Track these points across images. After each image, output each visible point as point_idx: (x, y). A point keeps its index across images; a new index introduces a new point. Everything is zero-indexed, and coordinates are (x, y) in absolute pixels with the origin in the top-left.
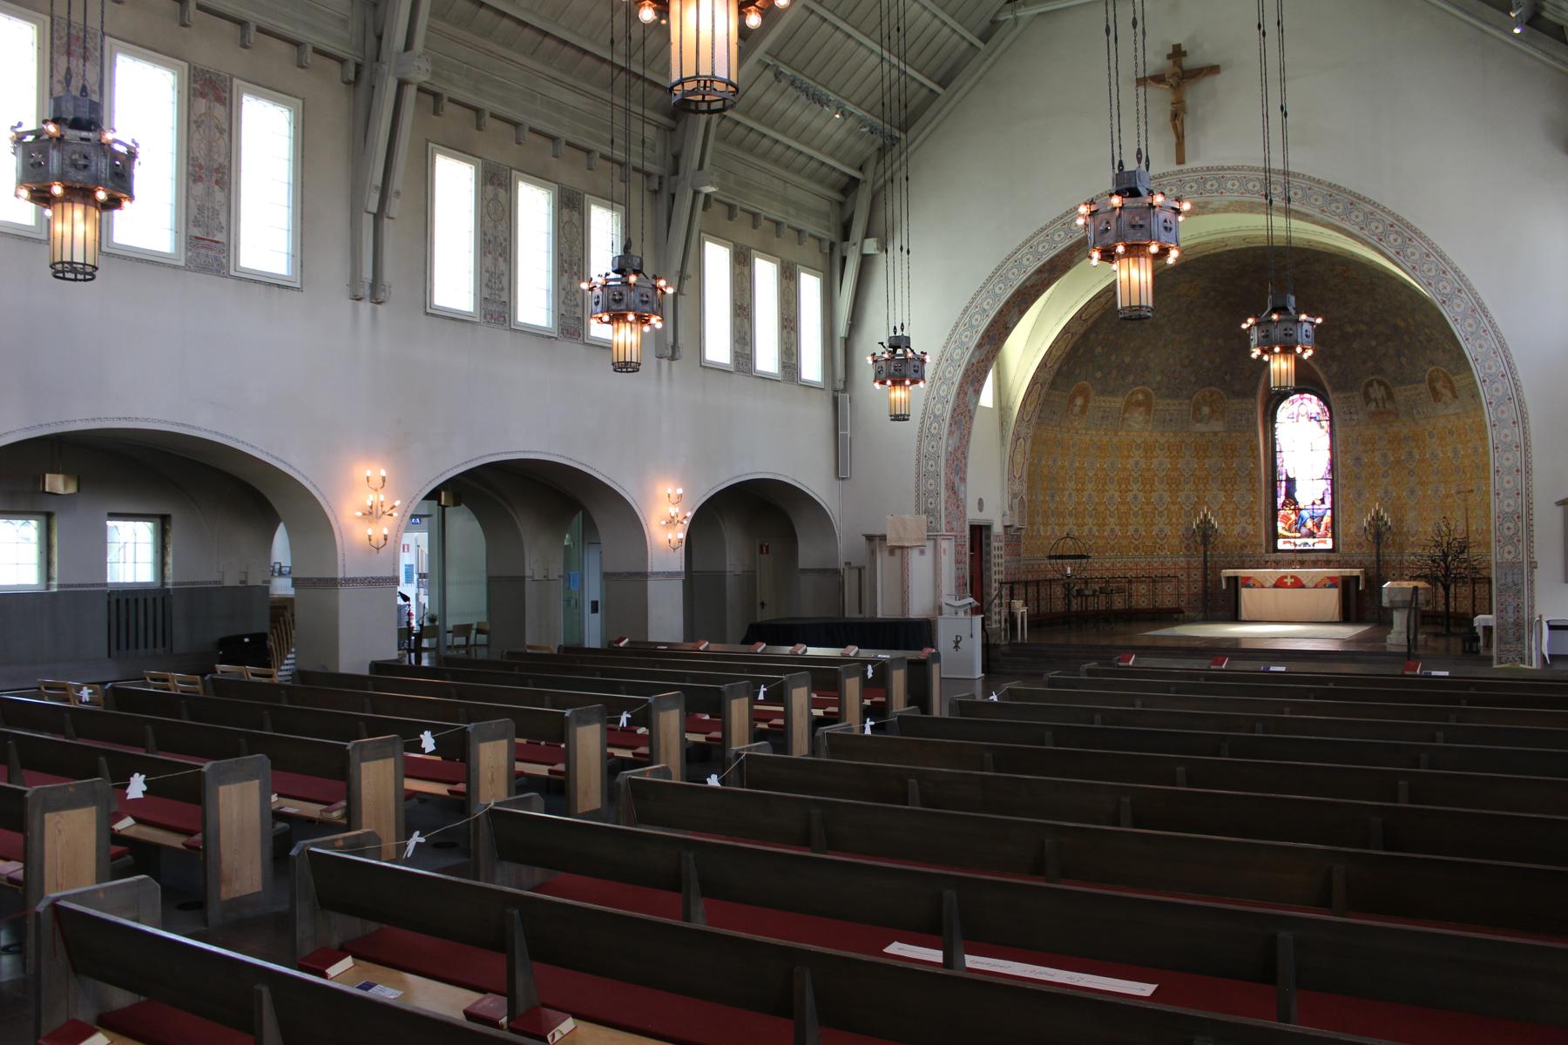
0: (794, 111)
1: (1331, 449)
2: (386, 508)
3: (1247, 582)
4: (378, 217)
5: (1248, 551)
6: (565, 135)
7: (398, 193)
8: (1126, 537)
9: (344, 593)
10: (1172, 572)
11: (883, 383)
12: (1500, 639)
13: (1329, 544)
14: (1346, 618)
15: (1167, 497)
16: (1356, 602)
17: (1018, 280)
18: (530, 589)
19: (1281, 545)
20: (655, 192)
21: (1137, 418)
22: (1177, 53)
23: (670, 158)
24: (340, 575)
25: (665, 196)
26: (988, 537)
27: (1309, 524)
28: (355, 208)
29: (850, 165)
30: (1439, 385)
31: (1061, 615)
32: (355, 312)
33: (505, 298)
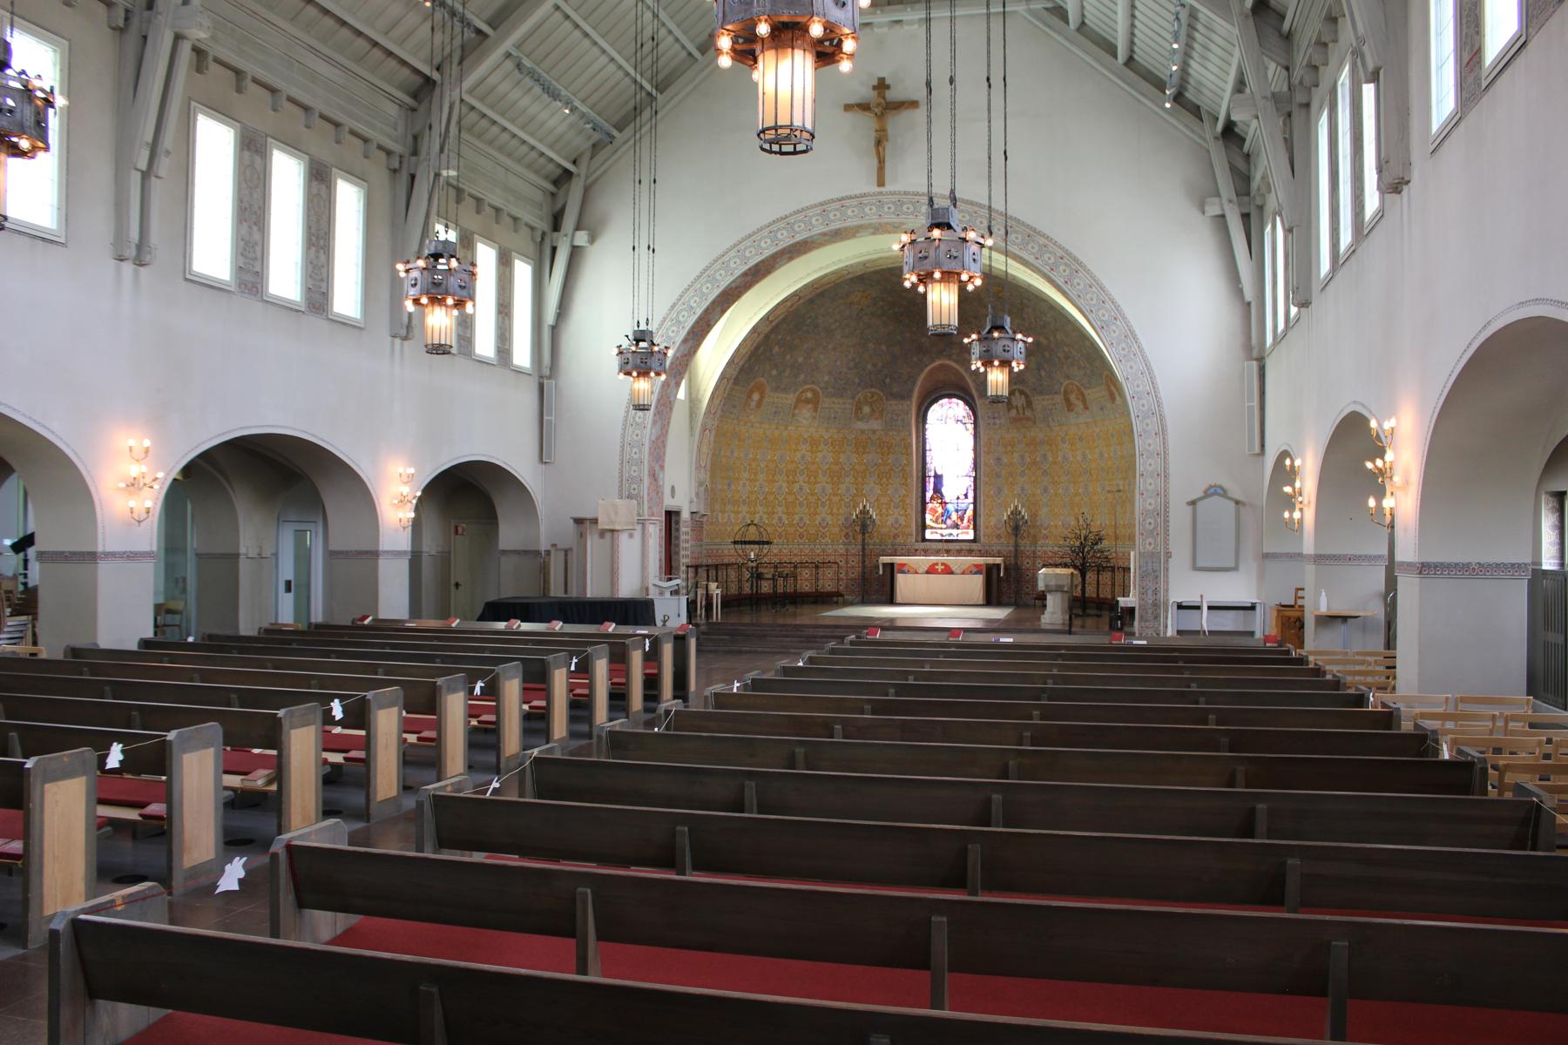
0: (515, 95)
1: (975, 450)
2: (148, 480)
3: (903, 569)
4: (146, 175)
5: (900, 540)
6: (318, 105)
7: (168, 152)
8: (791, 525)
9: (104, 568)
10: (831, 559)
11: (628, 374)
12: (1141, 617)
13: (971, 536)
14: (990, 600)
15: (829, 488)
16: (1005, 584)
17: (725, 281)
18: (244, 567)
19: (929, 535)
20: (395, 171)
21: (805, 413)
22: (882, 86)
23: (410, 140)
24: (100, 549)
25: (404, 177)
26: (677, 523)
27: (954, 516)
28: (121, 164)
29: (566, 158)
30: (1072, 397)
31: (753, 599)
32: (118, 271)
33: (258, 268)
